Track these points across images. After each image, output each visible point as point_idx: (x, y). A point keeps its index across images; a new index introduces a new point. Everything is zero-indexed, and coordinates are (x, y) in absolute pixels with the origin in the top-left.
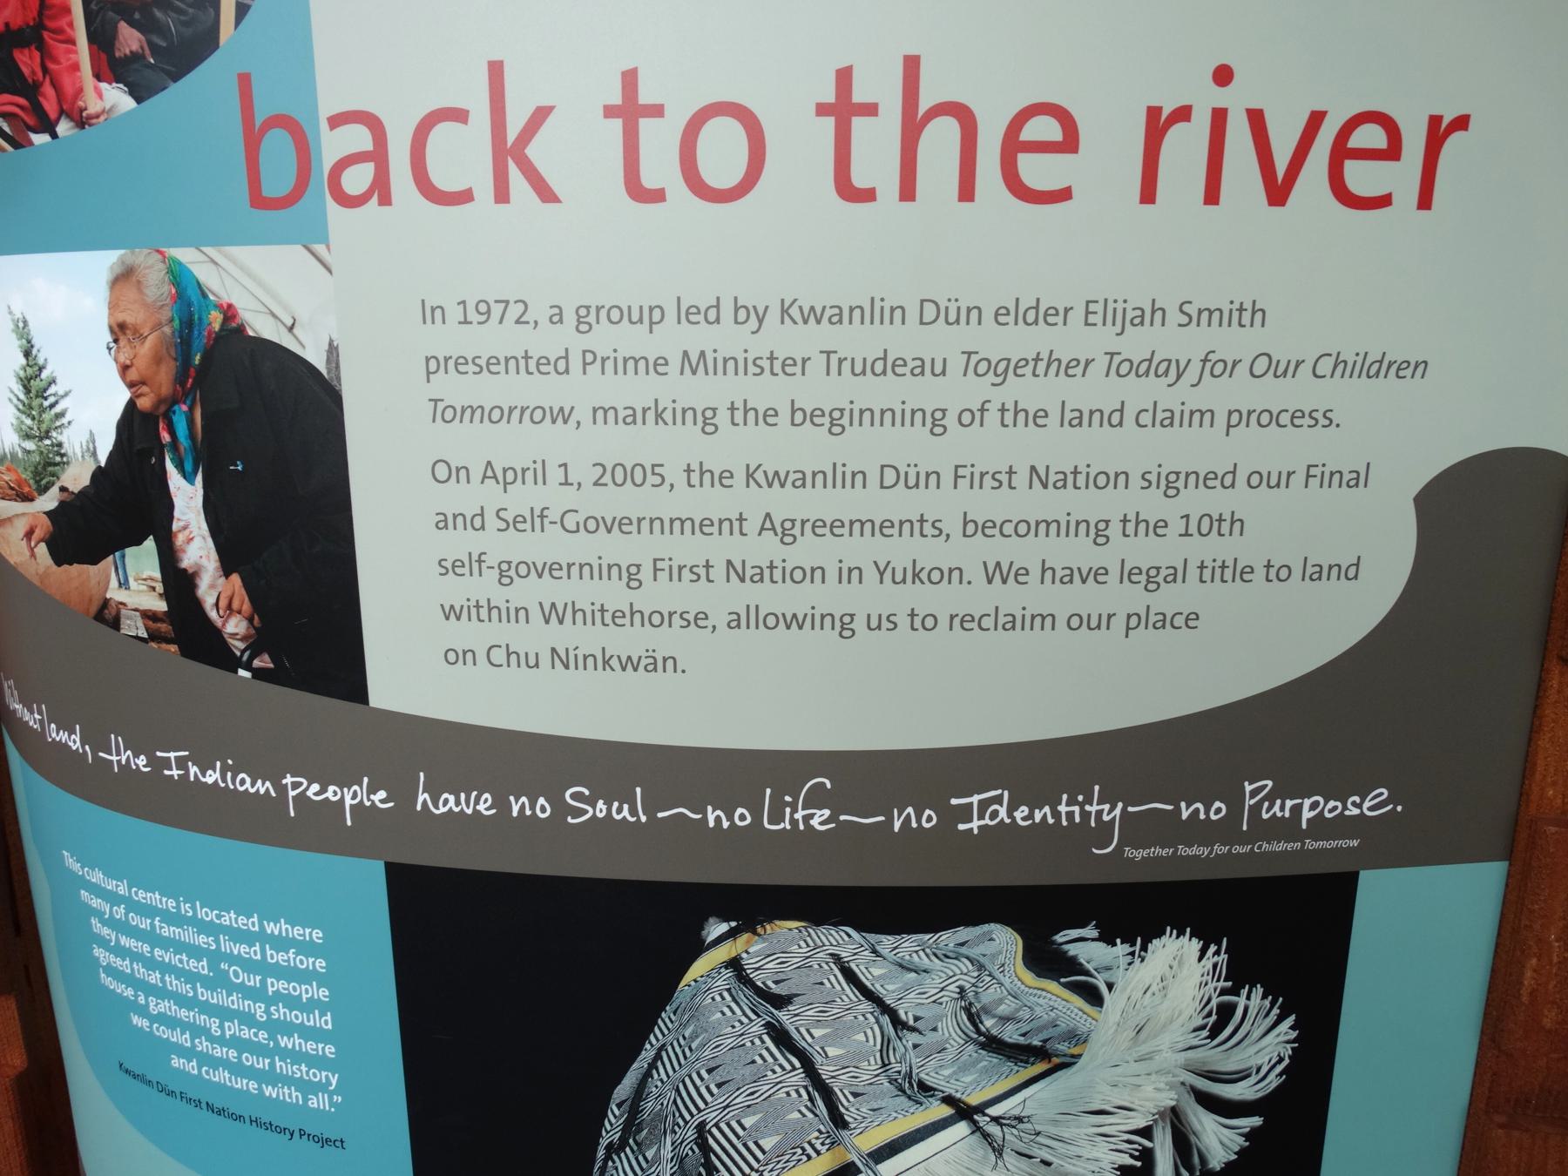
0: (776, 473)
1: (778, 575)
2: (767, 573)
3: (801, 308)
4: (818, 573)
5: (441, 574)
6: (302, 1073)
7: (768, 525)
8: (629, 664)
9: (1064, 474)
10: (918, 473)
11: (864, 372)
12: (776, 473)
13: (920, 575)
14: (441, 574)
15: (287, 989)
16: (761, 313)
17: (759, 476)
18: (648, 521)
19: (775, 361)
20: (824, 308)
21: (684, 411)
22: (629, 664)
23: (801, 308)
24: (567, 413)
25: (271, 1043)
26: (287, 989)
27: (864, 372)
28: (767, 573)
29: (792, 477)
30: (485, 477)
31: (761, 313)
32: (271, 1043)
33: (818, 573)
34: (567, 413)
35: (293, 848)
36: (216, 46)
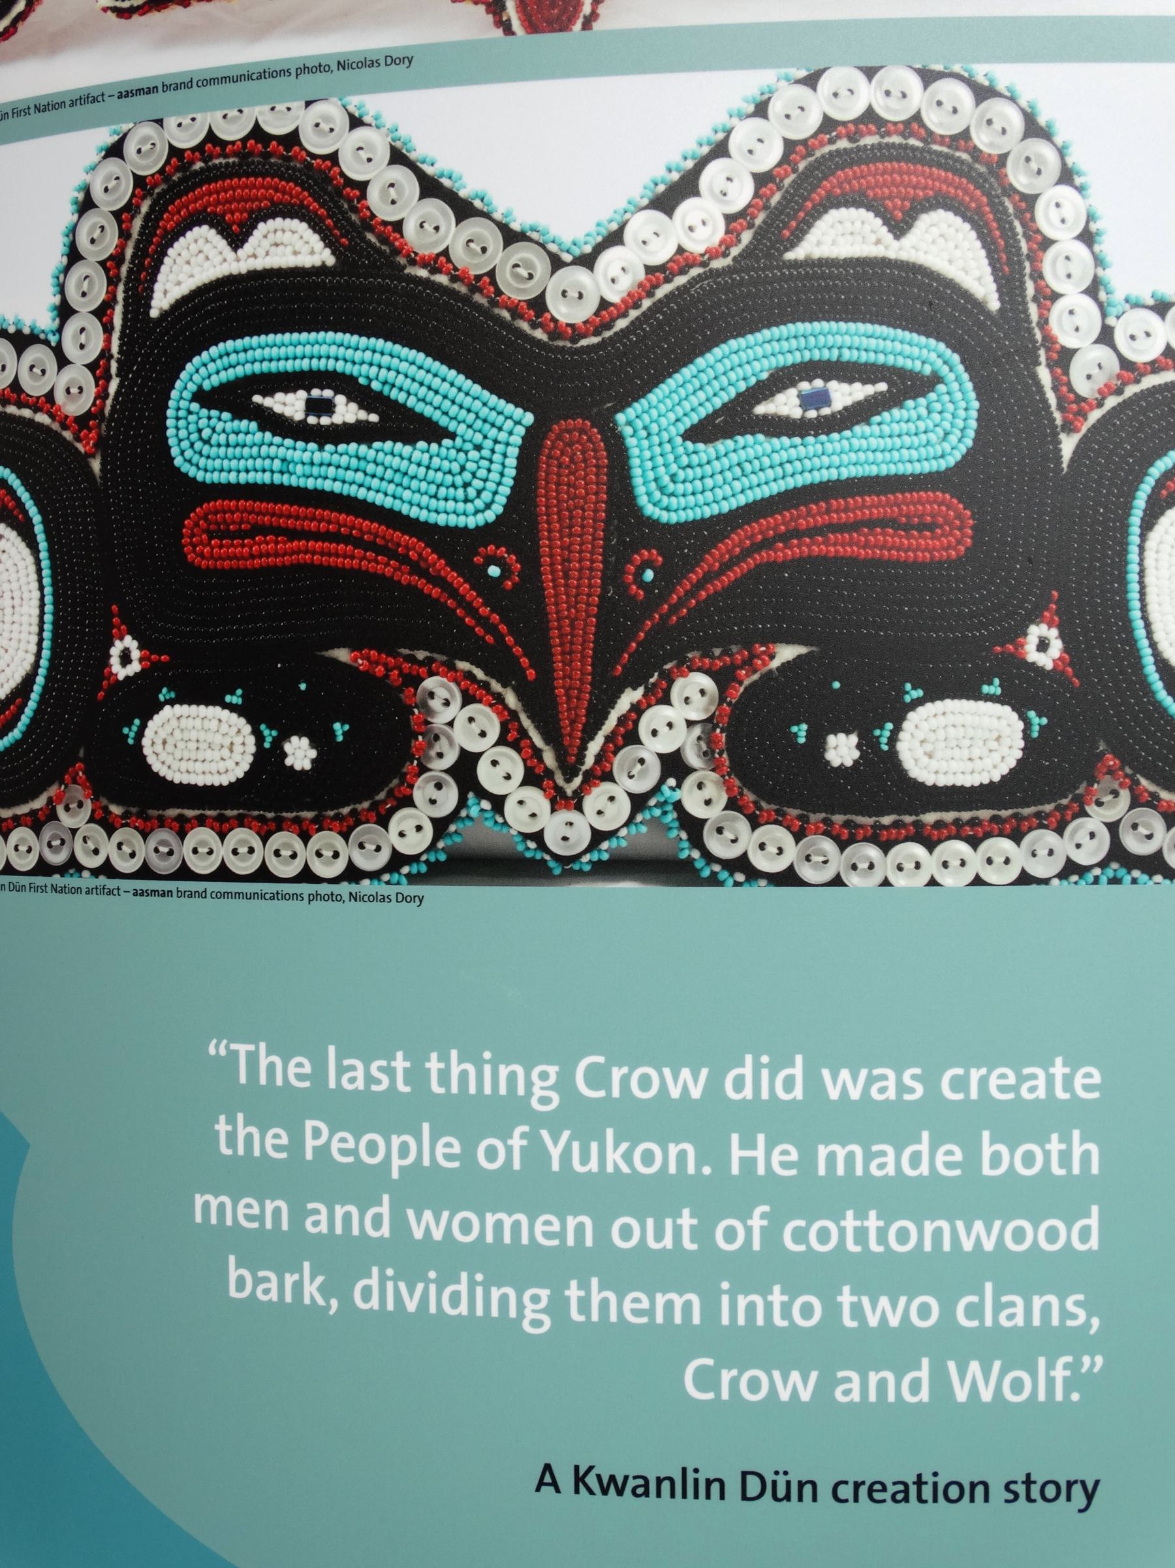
0: (612, 1478)
1: (927, 1492)
2: (913, 1490)
3: (599, 1477)
4: (980, 1490)
5: (1007, 1501)
6: (393, 1080)
7: (548, 1479)
8: (612, 1487)
9: (906, 1485)
10: (788, 1483)
11: (973, 1486)
12: (612, 1478)
13: (587, 1480)
14: (1007, 1501)
15: (354, 1152)
16: (1090, 1487)
17: (591, 1480)
18: (851, 1486)
19: (1033, 1486)
20: (626, 1478)
21: (709, 1483)
22: (612, 1487)
23: (599, 1477)
24: (620, 1481)
25: (334, 1303)
26: (354, 1152)
27: (973, 1486)
28: (913, 1490)
29: (631, 1483)
30: (541, 1483)
31: (1090, 1487)
32: (334, 1303)
33: (980, 1490)
34: (620, 1481)
35: (1106, 61)
36: (27, 1146)
